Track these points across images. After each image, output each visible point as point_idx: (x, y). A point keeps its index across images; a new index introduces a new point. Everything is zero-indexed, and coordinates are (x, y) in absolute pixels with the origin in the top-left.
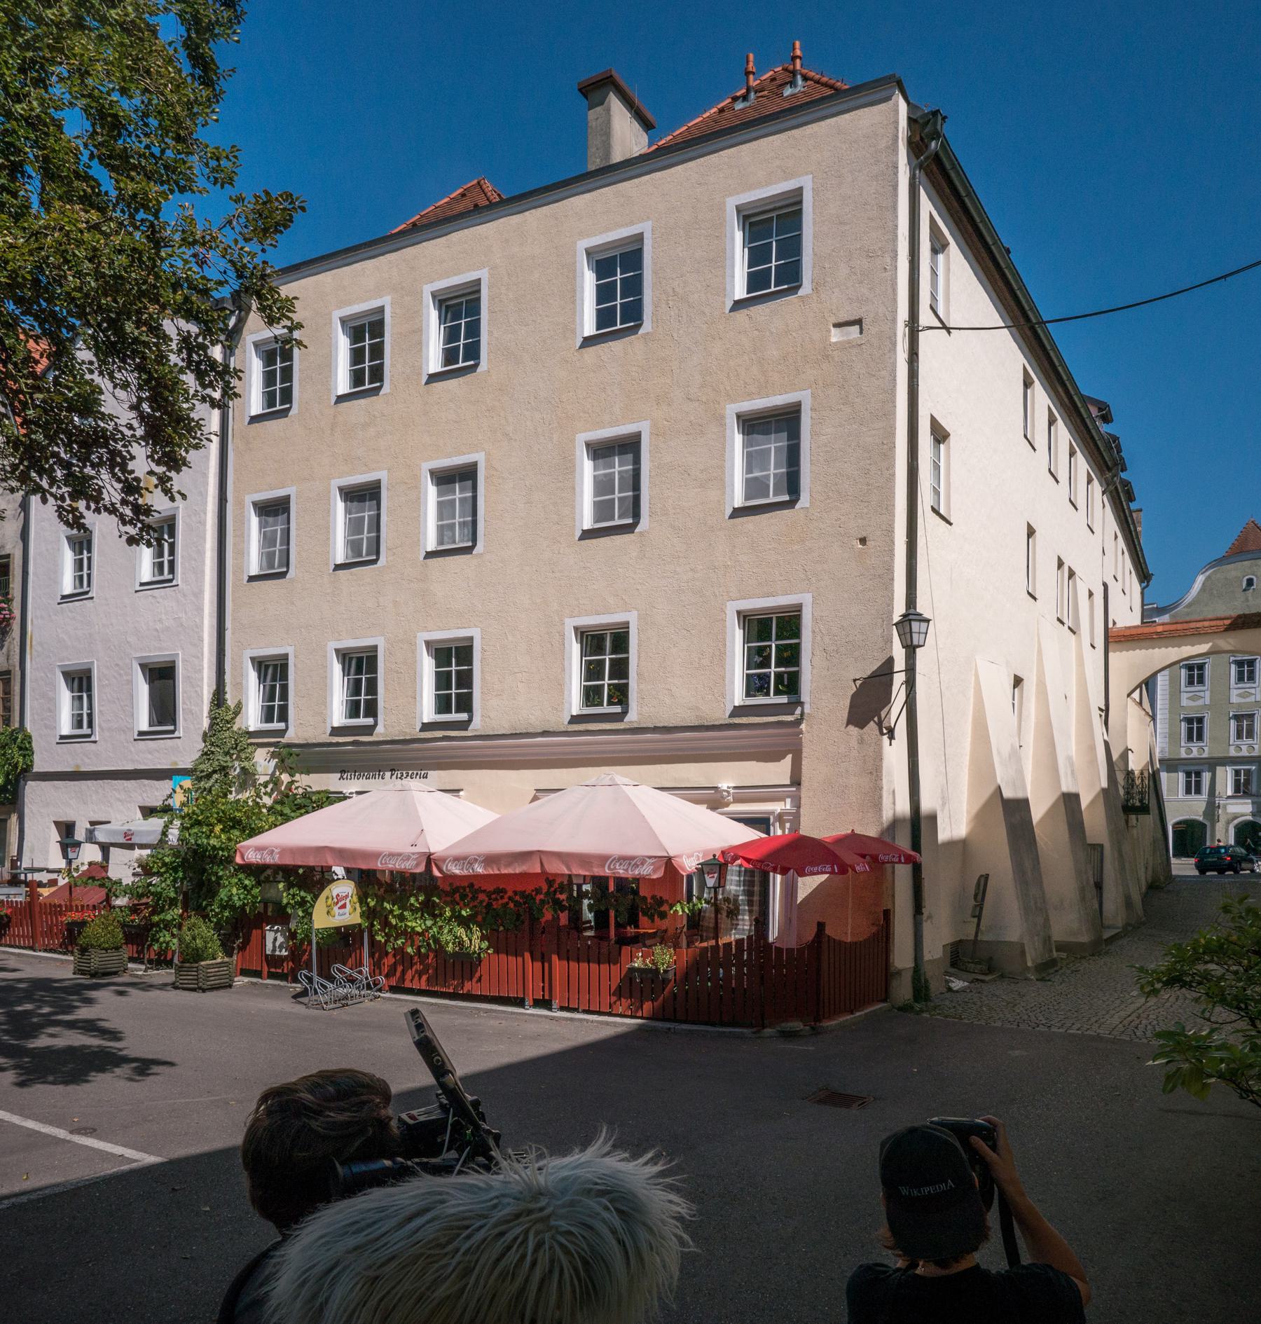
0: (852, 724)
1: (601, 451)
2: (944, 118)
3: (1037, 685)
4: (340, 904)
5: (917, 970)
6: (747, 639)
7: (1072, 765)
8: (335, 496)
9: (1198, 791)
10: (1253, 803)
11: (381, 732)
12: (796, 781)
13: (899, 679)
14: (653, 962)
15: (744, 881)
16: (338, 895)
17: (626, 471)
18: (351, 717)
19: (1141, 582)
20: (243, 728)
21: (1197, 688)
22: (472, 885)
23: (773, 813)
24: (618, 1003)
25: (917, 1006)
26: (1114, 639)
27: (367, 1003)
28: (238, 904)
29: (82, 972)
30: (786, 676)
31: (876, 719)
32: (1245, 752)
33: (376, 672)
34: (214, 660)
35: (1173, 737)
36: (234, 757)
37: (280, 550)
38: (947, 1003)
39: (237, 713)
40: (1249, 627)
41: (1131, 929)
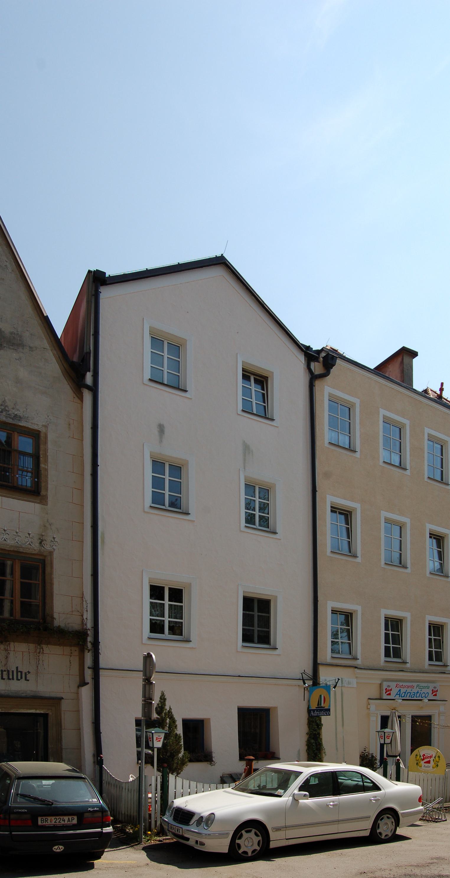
4: (425, 760)
16: (424, 755)
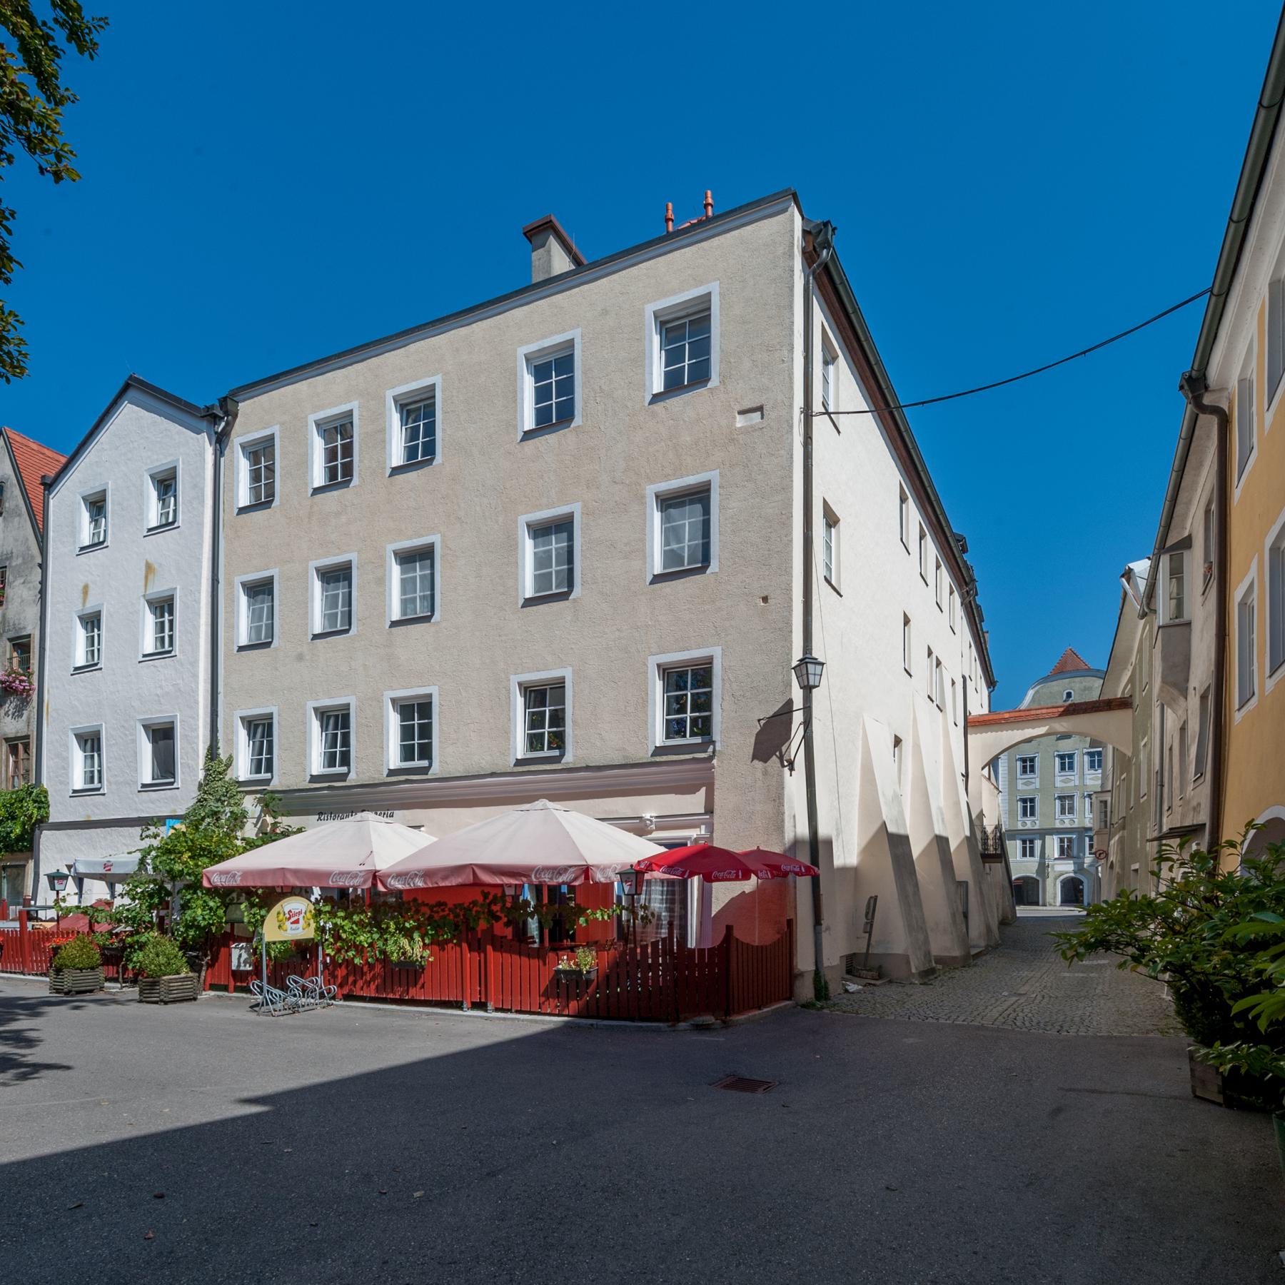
0: (758, 759)
1: (540, 531)
2: (834, 229)
3: (913, 747)
4: (293, 919)
5: (817, 973)
6: (667, 689)
7: (942, 814)
8: (313, 575)
9: (1032, 855)
10: (1074, 863)
11: (353, 778)
12: (709, 810)
13: (798, 717)
14: (577, 965)
15: (666, 899)
16: (290, 911)
17: (562, 548)
18: (329, 767)
19: (988, 687)
20: (234, 778)
21: (1029, 776)
22: (415, 900)
23: (689, 838)
24: (547, 1003)
25: (819, 1004)
26: (971, 724)
27: (319, 1010)
28: (203, 924)
29: (58, 991)
30: (700, 720)
31: (778, 754)
32: (1067, 825)
33: (349, 728)
34: (209, 720)
35: (1012, 813)
36: (226, 803)
37: (266, 625)
38: (845, 1001)
39: (228, 765)
40: (1078, 713)
41: (992, 948)
